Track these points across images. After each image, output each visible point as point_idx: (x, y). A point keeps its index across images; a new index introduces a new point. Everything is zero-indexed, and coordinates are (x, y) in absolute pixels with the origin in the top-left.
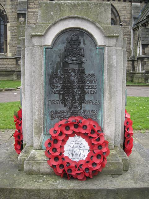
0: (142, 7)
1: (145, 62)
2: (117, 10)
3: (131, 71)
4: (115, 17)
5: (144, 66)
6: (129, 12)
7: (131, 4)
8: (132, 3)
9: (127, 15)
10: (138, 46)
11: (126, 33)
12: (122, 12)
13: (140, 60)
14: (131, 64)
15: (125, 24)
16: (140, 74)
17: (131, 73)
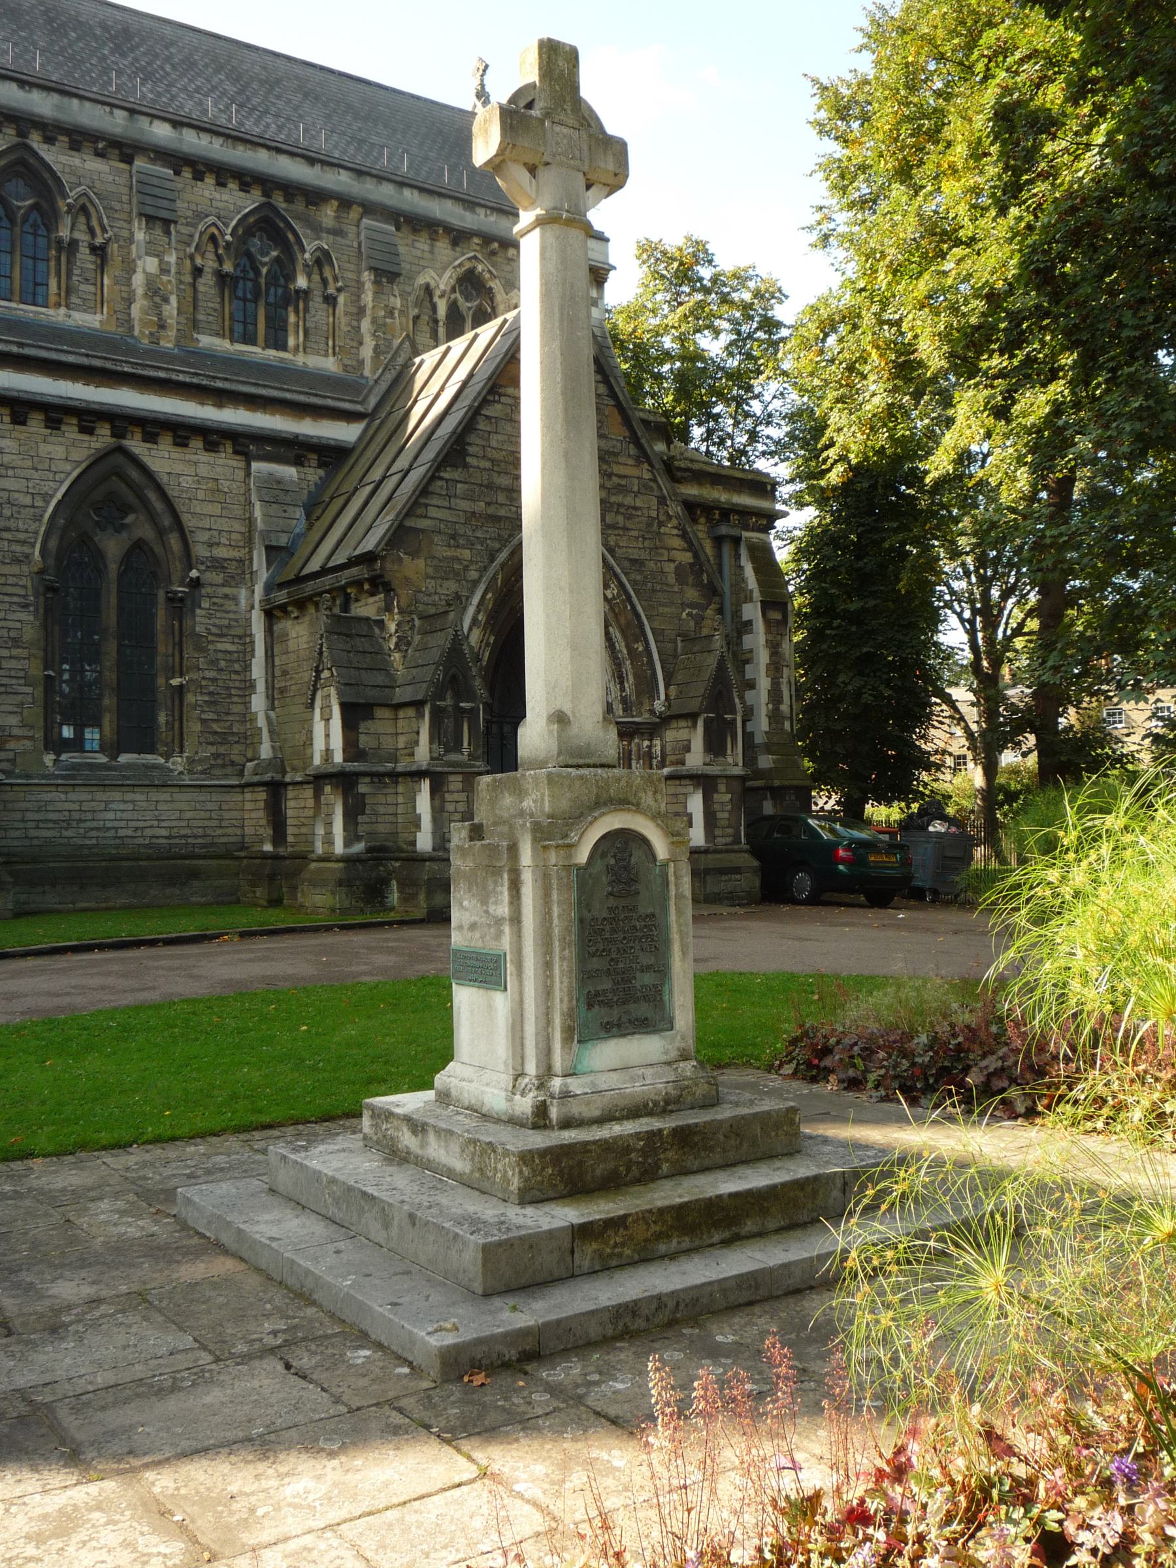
0: (305, 483)
1: (364, 795)
2: (170, 493)
3: (262, 842)
4: (161, 533)
5: (360, 818)
6: (238, 511)
7: (249, 466)
8: (255, 466)
9: (223, 524)
10: (317, 712)
11: (220, 627)
12: (198, 508)
13: (335, 786)
14: (262, 804)
15: (218, 578)
16: (341, 865)
17: (265, 856)
